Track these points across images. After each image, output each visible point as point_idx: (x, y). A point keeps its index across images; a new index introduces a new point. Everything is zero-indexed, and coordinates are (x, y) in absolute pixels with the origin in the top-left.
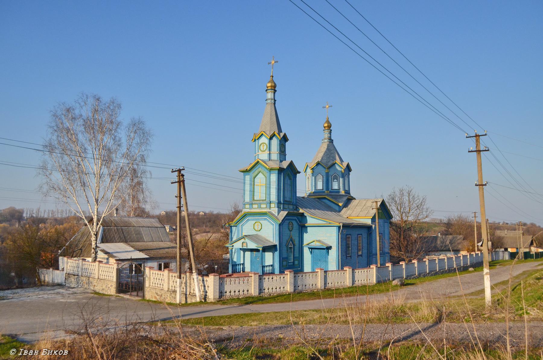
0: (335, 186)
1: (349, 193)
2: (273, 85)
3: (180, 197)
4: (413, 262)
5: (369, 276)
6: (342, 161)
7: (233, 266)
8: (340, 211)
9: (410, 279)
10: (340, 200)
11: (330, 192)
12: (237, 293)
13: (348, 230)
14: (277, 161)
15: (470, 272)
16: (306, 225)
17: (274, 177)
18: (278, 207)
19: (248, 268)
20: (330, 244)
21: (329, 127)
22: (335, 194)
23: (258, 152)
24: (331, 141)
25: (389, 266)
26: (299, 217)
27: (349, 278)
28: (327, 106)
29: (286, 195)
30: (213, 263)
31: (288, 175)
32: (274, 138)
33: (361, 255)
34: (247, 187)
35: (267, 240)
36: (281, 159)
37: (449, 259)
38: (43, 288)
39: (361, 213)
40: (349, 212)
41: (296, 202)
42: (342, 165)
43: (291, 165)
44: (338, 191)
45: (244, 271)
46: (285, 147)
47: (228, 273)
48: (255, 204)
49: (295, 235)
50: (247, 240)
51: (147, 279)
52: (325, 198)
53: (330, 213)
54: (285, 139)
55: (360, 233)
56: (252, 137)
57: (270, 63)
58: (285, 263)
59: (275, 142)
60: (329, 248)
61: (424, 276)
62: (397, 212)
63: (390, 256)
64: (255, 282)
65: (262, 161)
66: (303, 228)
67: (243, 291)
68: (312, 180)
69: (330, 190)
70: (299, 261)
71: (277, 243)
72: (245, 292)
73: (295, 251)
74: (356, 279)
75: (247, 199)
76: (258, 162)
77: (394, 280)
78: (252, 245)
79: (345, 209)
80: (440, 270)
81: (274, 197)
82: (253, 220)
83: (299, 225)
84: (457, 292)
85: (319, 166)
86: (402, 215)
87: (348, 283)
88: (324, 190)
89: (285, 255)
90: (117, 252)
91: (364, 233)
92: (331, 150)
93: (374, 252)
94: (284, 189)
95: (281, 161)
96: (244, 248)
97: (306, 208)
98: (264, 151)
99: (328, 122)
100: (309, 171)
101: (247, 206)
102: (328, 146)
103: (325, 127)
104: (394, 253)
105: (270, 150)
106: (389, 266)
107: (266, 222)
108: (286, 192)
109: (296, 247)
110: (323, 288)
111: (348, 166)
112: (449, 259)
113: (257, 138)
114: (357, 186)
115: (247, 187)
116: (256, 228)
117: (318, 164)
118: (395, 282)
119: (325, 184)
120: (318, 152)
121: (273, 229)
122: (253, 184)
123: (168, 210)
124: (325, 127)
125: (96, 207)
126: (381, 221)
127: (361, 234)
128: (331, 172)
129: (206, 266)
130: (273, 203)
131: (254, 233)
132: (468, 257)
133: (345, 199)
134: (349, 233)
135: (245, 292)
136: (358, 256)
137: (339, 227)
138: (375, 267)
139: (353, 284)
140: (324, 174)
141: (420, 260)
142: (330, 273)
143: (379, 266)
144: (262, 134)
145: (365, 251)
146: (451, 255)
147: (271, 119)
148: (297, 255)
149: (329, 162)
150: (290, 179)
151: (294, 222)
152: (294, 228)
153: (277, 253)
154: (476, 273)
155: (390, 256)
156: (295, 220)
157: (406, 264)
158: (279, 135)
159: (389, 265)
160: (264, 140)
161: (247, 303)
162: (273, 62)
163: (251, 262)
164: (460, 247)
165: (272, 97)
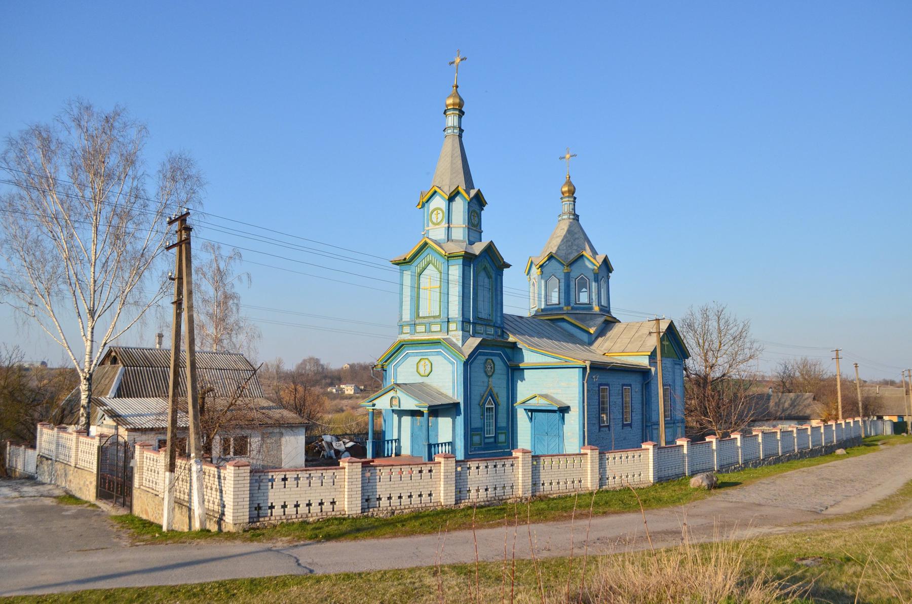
0: (584, 298)
1: (609, 312)
2: (457, 101)
3: (180, 278)
4: (732, 436)
5: (638, 466)
6: (594, 253)
8: (591, 343)
9: (727, 472)
10: (592, 323)
11: (573, 308)
12: (303, 509)
13: (600, 374)
14: (463, 241)
15: (840, 457)
16: (522, 365)
17: (456, 271)
18: (463, 330)
19: (406, 450)
20: (567, 402)
21: (572, 192)
22: (584, 313)
23: (428, 226)
24: (576, 218)
25: (831, 425)
26: (508, 351)
27: (592, 471)
28: (568, 156)
31: (485, 269)
32: (458, 199)
33: (630, 425)
34: (407, 292)
35: (442, 394)
36: (472, 239)
37: (784, 433)
38: (13, 483)
39: (630, 346)
40: (607, 345)
41: (503, 322)
42: (595, 258)
43: (490, 250)
44: (589, 307)
45: (398, 454)
48: (420, 324)
49: (498, 384)
50: (400, 394)
51: (135, 470)
52: (563, 320)
53: (570, 345)
54: (478, 202)
55: (626, 381)
56: (417, 199)
57: (453, 63)
58: (476, 439)
59: (460, 207)
60: (564, 410)
61: (755, 466)
62: (697, 350)
63: (686, 427)
64: (351, 483)
65: (435, 242)
66: (515, 371)
67: (321, 504)
68: (540, 287)
69: (572, 305)
71: (460, 399)
72: (327, 507)
73: (500, 415)
74: (609, 473)
75: (407, 317)
76: (426, 244)
77: (693, 474)
78: (409, 403)
79: (600, 340)
80: (784, 453)
81: (455, 311)
82: (417, 354)
84: (837, 503)
85: (553, 261)
86: (706, 354)
87: (590, 482)
88: (562, 305)
89: (476, 423)
90: (133, 416)
91: (636, 382)
92: (576, 235)
93: (654, 419)
94: (475, 294)
95: (471, 243)
97: (522, 334)
98: (438, 224)
99: (569, 183)
100: (535, 271)
101: (407, 329)
102: (570, 226)
103: (563, 193)
104: (692, 422)
105: (449, 221)
106: (831, 425)
107: (439, 358)
109: (500, 408)
110: (529, 495)
111: (606, 261)
112: (784, 433)
114: (622, 297)
115: (407, 292)
117: (551, 257)
118: (697, 481)
119: (562, 295)
120: (553, 238)
121: (453, 373)
122: (416, 288)
123: (356, 362)
124: (563, 193)
125: (90, 324)
126: (669, 362)
127: (630, 385)
128: (576, 272)
129: (350, 444)
130: (454, 322)
131: (418, 379)
132: (822, 430)
133: (601, 320)
134: (604, 381)
135: (327, 507)
136: (624, 425)
137: (584, 369)
138: (651, 447)
139: (601, 486)
140: (562, 276)
141: (746, 434)
142: (547, 460)
143: (663, 444)
144: (435, 192)
145: (637, 417)
146: (792, 427)
147: (452, 163)
148: (502, 423)
149: (571, 253)
150: (489, 277)
151: (497, 361)
152: (496, 371)
153: (460, 419)
154: (852, 459)
155: (686, 427)
156: (499, 355)
157: (720, 441)
158: (468, 193)
159: (682, 442)
160: (439, 202)
161: (329, 537)
162: (458, 60)
163: (412, 436)
164: (808, 412)
165: (456, 124)
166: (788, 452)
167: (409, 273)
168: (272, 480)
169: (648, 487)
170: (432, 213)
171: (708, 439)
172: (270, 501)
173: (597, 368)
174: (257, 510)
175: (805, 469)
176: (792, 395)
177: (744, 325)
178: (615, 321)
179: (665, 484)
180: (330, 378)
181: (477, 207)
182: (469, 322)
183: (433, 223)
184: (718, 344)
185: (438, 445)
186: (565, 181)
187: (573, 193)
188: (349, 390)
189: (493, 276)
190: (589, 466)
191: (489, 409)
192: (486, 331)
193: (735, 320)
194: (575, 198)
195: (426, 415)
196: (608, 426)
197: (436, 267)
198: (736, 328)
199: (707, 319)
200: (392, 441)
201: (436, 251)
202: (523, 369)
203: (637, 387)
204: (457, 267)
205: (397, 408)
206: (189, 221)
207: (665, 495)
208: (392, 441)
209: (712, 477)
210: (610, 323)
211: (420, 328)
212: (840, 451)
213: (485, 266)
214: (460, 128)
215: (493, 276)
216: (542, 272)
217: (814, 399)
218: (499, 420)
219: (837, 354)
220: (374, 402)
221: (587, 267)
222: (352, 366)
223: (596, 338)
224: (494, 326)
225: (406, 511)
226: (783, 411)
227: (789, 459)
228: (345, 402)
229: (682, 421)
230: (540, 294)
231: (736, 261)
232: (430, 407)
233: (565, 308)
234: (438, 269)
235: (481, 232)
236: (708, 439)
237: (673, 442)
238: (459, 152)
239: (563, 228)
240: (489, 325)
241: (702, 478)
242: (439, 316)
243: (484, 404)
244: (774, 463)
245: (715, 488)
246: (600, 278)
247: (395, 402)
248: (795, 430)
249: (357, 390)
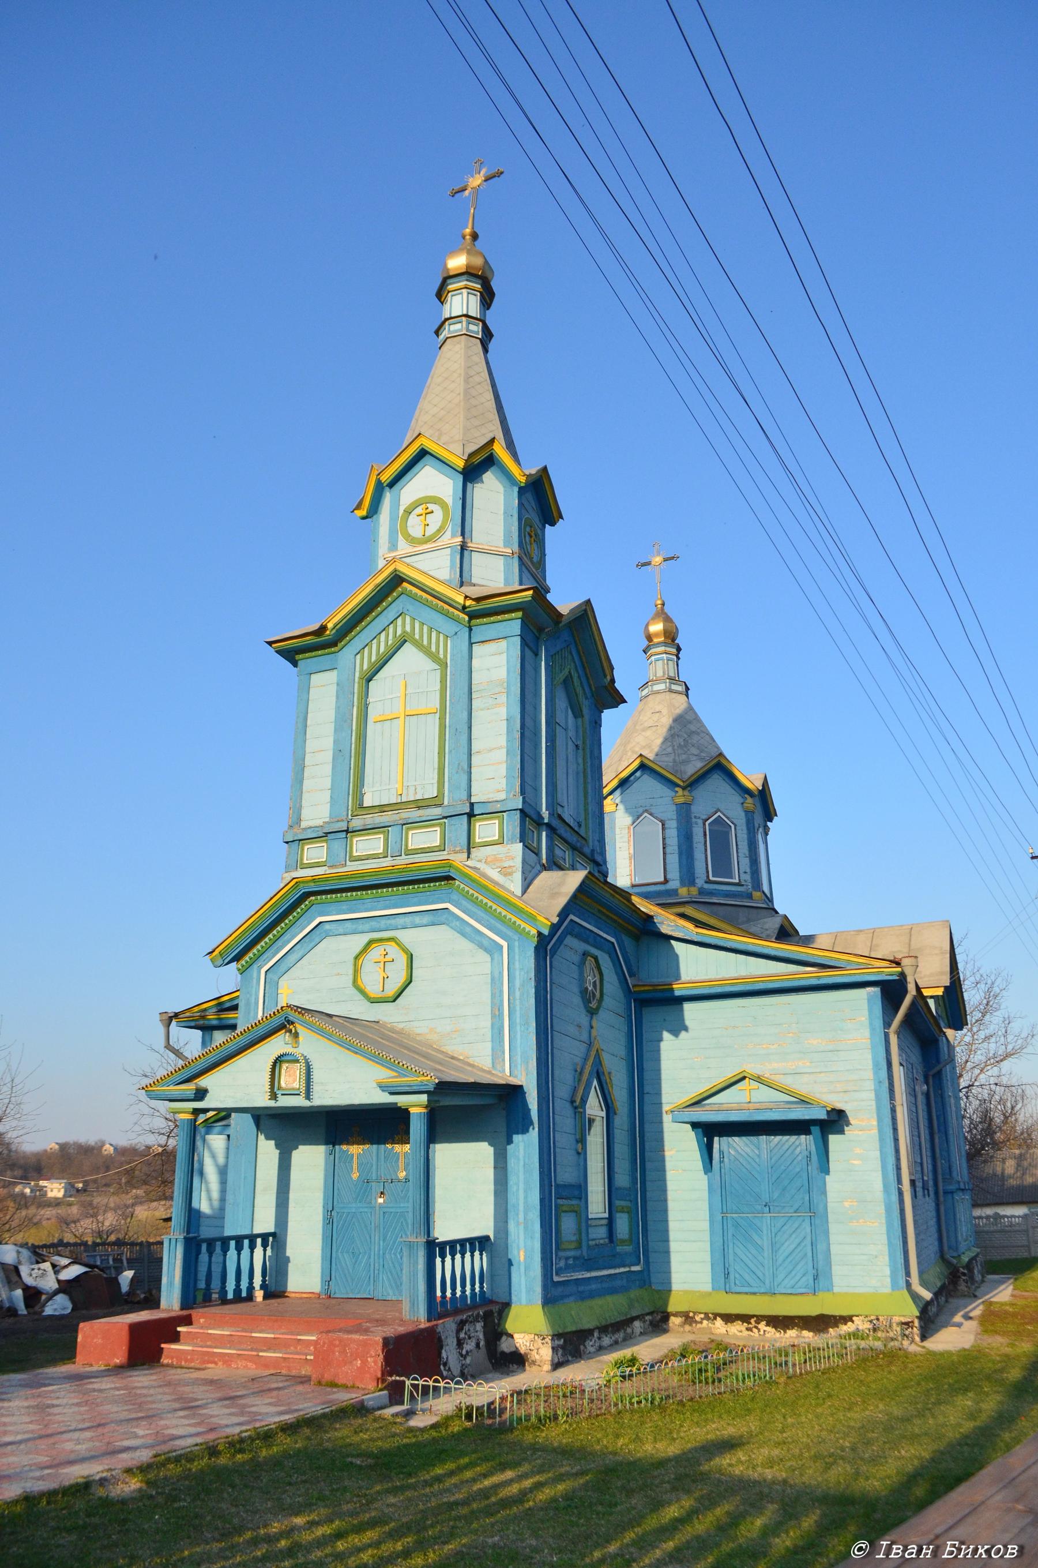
7: (193, 1246)
11: (702, 892)
18: (522, 839)
19: (305, 1276)
21: (671, 636)
23: (393, 546)
28: (658, 560)
29: (562, 797)
30: (118, 1260)
32: (490, 478)
45: (275, 1292)
46: (540, 542)
47: (152, 1301)
49: (609, 1032)
59: (494, 501)
60: (835, 1121)
66: (657, 1003)
69: (700, 882)
70: (631, 1212)
71: (525, 1076)
78: (348, 1081)
81: (495, 776)
83: (628, 991)
88: (674, 884)
96: (285, 1102)
108: (561, 763)
113: (386, 477)
116: (372, 979)
119: (674, 860)
121: (495, 981)
124: (649, 638)
129: (74, 1271)
140: (670, 813)
147: (468, 395)
149: (686, 762)
150: (577, 713)
153: (525, 1147)
167: (332, 677)
170: (408, 512)
180: (21, 1167)
183: (412, 540)
185: (225, 1241)
187: (673, 640)
188: (55, 1189)
194: (679, 649)
195: (417, 1128)
197: (426, 651)
200: (252, 1238)
205: (299, 1102)
220: (204, 1082)
222: (63, 1147)
228: (48, 1212)
233: (683, 891)
234: (434, 657)
247: (291, 1078)
249: (70, 1189)
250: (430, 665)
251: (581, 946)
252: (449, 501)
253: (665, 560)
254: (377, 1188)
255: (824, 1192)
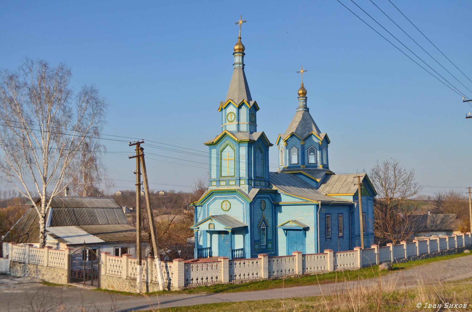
0: (312, 160)
1: (328, 168)
3: (140, 174)
4: (401, 243)
5: (352, 259)
6: (319, 132)
7: (198, 250)
8: (317, 188)
10: (318, 176)
11: (306, 167)
12: (205, 280)
13: (327, 209)
14: (246, 132)
15: (466, 254)
16: (280, 203)
17: (243, 151)
20: (308, 225)
21: (305, 94)
22: (312, 169)
23: (226, 122)
26: (272, 195)
28: (302, 71)
31: (260, 148)
32: (243, 107)
33: (342, 237)
34: (214, 162)
36: (252, 130)
37: (431, 241)
39: (342, 189)
40: (328, 189)
42: (319, 136)
43: (263, 136)
44: (315, 165)
45: (211, 256)
46: (255, 116)
48: (223, 181)
49: (268, 214)
50: (214, 221)
53: (306, 190)
54: (255, 108)
55: (340, 211)
56: (218, 106)
59: (244, 111)
60: (306, 229)
61: (414, 259)
62: (381, 189)
63: (375, 237)
64: (224, 268)
68: (286, 153)
69: (306, 164)
71: (248, 224)
72: (214, 279)
74: (338, 263)
75: (214, 176)
76: (225, 134)
77: (380, 263)
78: (220, 227)
79: (323, 185)
80: (431, 252)
81: (244, 173)
82: (221, 198)
85: (294, 138)
87: (329, 268)
88: (300, 164)
89: (257, 238)
91: (345, 212)
92: (307, 120)
93: (356, 233)
95: (251, 133)
96: (211, 230)
97: (280, 185)
98: (232, 122)
99: (303, 88)
100: (282, 143)
102: (303, 115)
103: (299, 94)
104: (379, 234)
105: (238, 120)
110: (301, 273)
112: (431, 241)
116: (224, 207)
117: (292, 135)
118: (383, 266)
119: (300, 158)
120: (293, 123)
121: (244, 209)
122: (220, 159)
124: (299, 94)
126: (364, 198)
127: (342, 214)
131: (223, 213)
133: (323, 174)
135: (214, 279)
137: (318, 206)
138: (359, 250)
140: (300, 147)
141: (409, 242)
142: (309, 257)
143: (363, 249)
144: (230, 103)
145: (346, 232)
147: (239, 85)
148: (270, 237)
150: (262, 152)
151: (267, 201)
153: (248, 236)
156: (268, 198)
157: (394, 246)
158: (249, 104)
160: (232, 109)
161: (217, 292)
162: (241, 22)
163: (219, 245)
164: (453, 226)
165: (241, 61)
166: (434, 252)
168: (236, 264)
169: (357, 270)
170: (228, 115)
171: (388, 245)
172: (192, 277)
173: (325, 204)
174: (187, 280)
175: (442, 261)
176: (442, 215)
177: (411, 173)
178: (332, 174)
179: (366, 269)
181: (254, 111)
182: (252, 179)
184: (394, 184)
185: (203, 249)
186: (300, 86)
189: (264, 152)
190: (329, 260)
191: (263, 229)
192: (260, 184)
193: (405, 170)
194: (306, 98)
196: (330, 238)
197: (232, 147)
198: (405, 175)
199: (387, 169)
200: (207, 248)
201: (231, 138)
202: (281, 206)
203: (346, 214)
204: (244, 148)
205: (213, 230)
206: (141, 145)
207: (366, 273)
208: (203, 249)
209: (390, 265)
210: (328, 175)
211: (223, 183)
212: (466, 251)
213: (260, 147)
214: (243, 63)
215: (264, 152)
216: (287, 144)
217: (457, 218)
218: (268, 236)
219: (470, 190)
220: (199, 226)
221: (314, 141)
222: (122, 193)
223: (321, 185)
224: (265, 181)
225: (247, 281)
226: (436, 226)
227: (434, 256)
229: (372, 234)
230: (285, 158)
231: (406, 135)
232: (233, 229)
233: (302, 166)
235: (256, 126)
236: (388, 245)
237: (370, 246)
238: (243, 78)
239: (299, 117)
240: (262, 181)
241: (385, 265)
242: (234, 176)
243: (260, 226)
244: (425, 258)
245: (392, 270)
246: (322, 147)
247: (212, 226)
248: (438, 239)
250: (232, 150)
251: (260, 200)
252: (235, 113)
253: (304, 71)
254: (226, 240)
255: (305, 241)
